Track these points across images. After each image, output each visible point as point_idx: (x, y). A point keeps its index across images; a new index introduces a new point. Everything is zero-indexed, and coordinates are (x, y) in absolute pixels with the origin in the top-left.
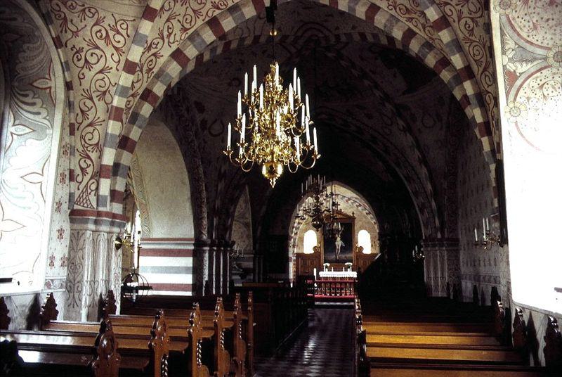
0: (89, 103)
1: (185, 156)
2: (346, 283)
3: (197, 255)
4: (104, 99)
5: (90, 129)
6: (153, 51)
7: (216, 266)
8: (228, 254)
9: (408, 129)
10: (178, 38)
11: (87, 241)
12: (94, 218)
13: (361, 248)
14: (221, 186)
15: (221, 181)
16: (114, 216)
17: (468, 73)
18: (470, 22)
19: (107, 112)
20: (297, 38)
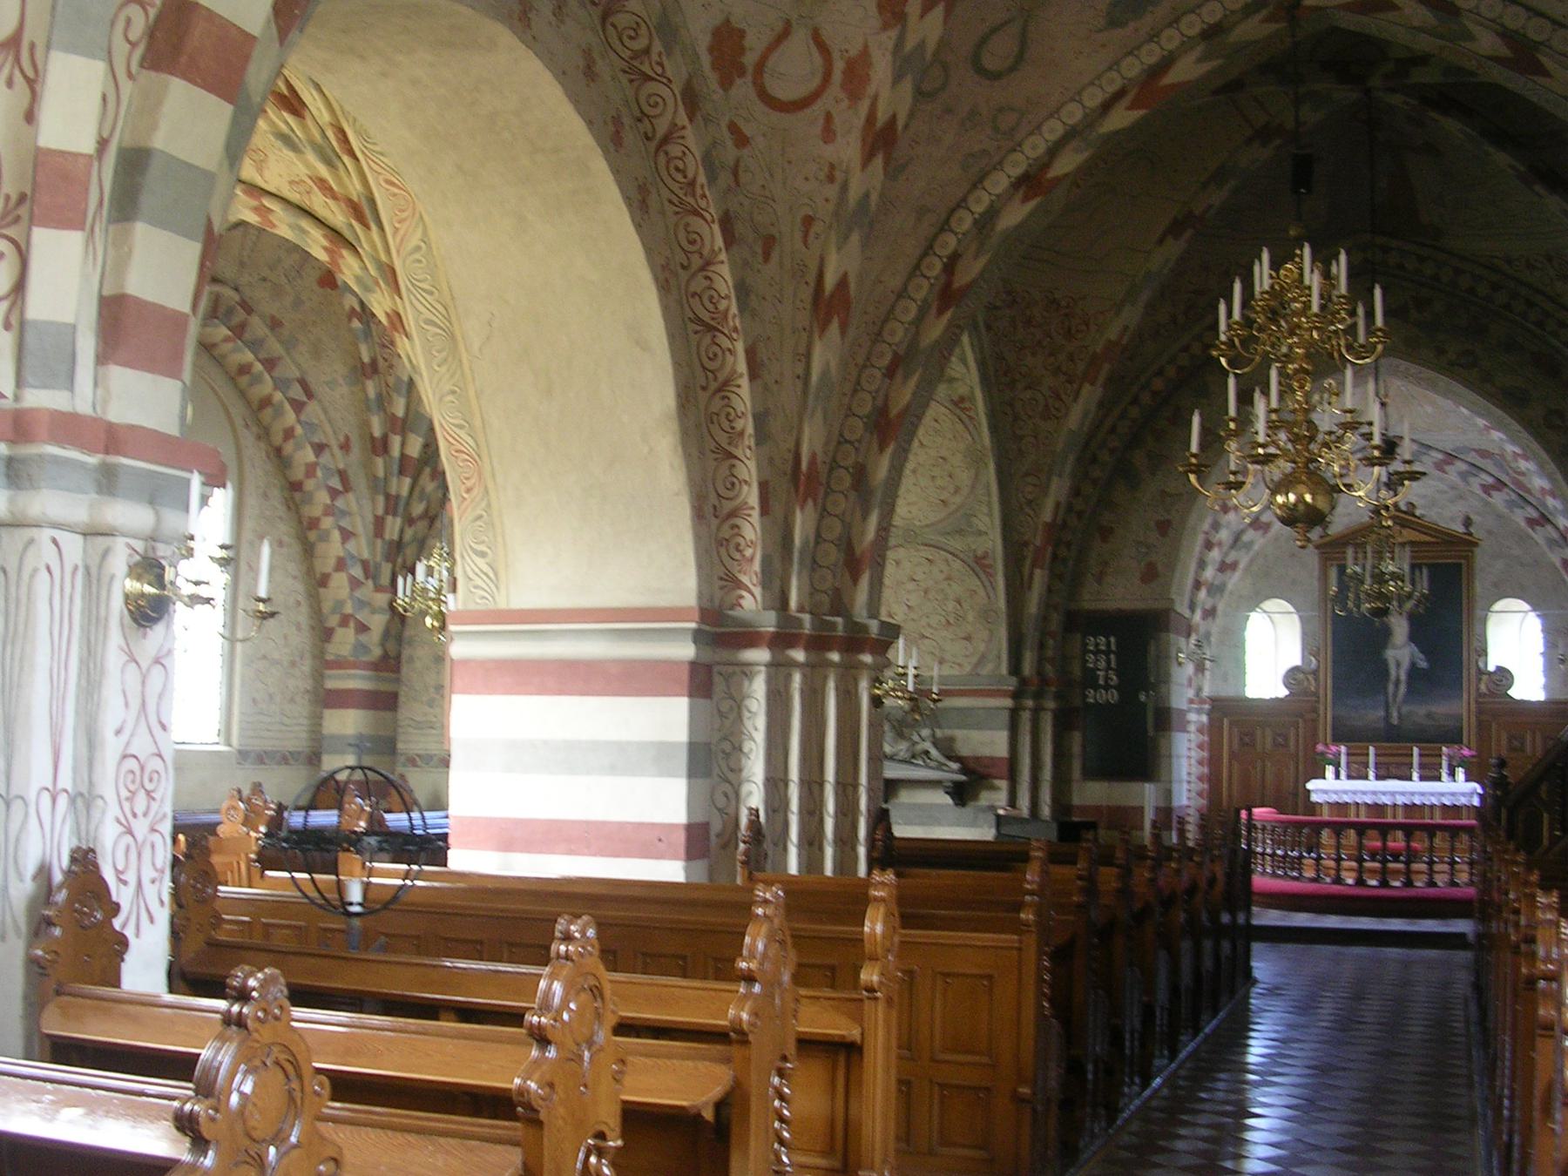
1: (640, 202)
2: (1431, 830)
3: (707, 682)
7: (870, 748)
8: (864, 685)
12: (93, 460)
13: (1504, 676)
14: (826, 354)
15: (823, 329)
16: (112, 438)
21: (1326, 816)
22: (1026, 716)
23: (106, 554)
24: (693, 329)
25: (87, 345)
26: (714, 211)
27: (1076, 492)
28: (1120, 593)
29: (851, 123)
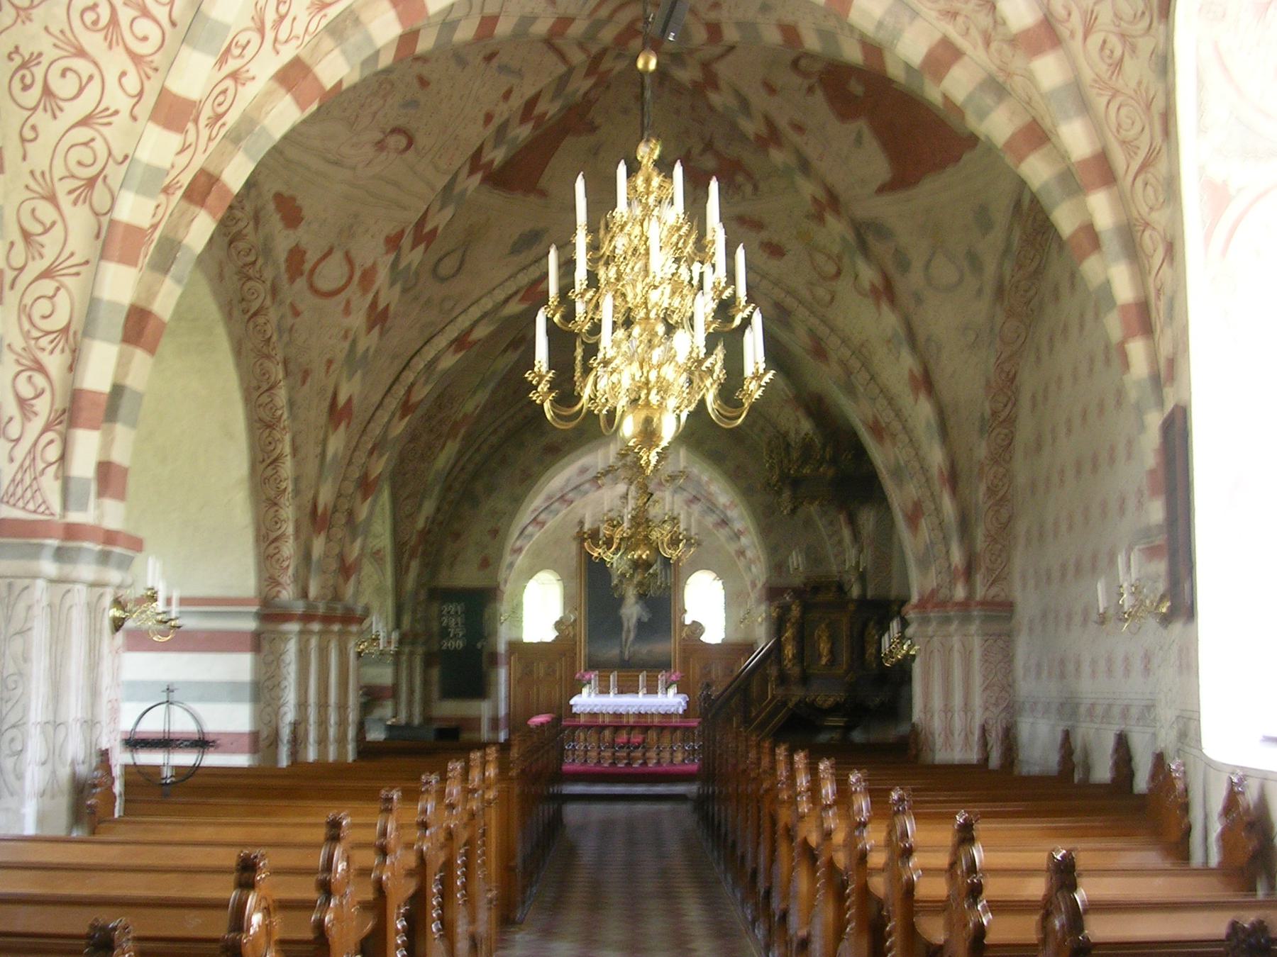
0: (46, 211)
1: (238, 351)
4: (88, 200)
5: (47, 286)
6: (232, 65)
9: (887, 292)
10: (299, 29)
11: (37, 610)
12: (99, 547)
13: (697, 628)
14: (336, 443)
15: (336, 427)
17: (1102, 170)
18: (1115, 42)
19: (98, 236)
20: (597, 26)
21: (582, 720)
22: (404, 658)
23: (101, 595)
24: (262, 426)
25: (93, 488)
26: (279, 357)
27: (438, 510)
28: (466, 576)
29: (361, 305)
